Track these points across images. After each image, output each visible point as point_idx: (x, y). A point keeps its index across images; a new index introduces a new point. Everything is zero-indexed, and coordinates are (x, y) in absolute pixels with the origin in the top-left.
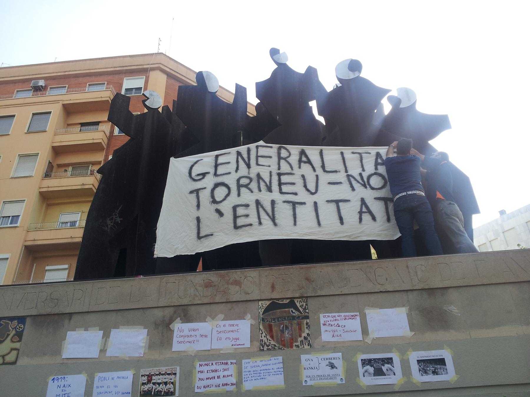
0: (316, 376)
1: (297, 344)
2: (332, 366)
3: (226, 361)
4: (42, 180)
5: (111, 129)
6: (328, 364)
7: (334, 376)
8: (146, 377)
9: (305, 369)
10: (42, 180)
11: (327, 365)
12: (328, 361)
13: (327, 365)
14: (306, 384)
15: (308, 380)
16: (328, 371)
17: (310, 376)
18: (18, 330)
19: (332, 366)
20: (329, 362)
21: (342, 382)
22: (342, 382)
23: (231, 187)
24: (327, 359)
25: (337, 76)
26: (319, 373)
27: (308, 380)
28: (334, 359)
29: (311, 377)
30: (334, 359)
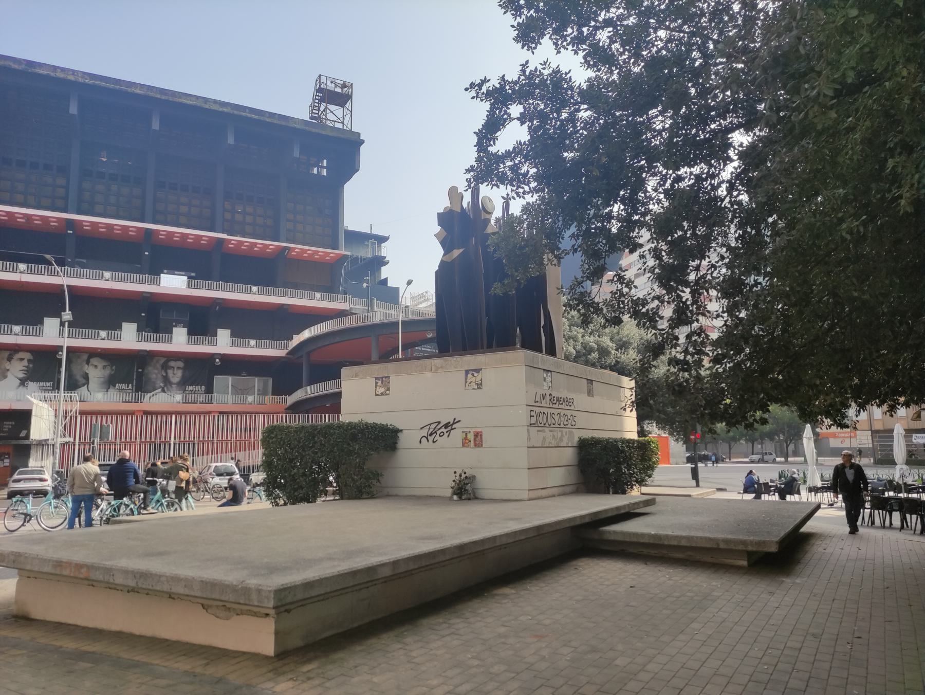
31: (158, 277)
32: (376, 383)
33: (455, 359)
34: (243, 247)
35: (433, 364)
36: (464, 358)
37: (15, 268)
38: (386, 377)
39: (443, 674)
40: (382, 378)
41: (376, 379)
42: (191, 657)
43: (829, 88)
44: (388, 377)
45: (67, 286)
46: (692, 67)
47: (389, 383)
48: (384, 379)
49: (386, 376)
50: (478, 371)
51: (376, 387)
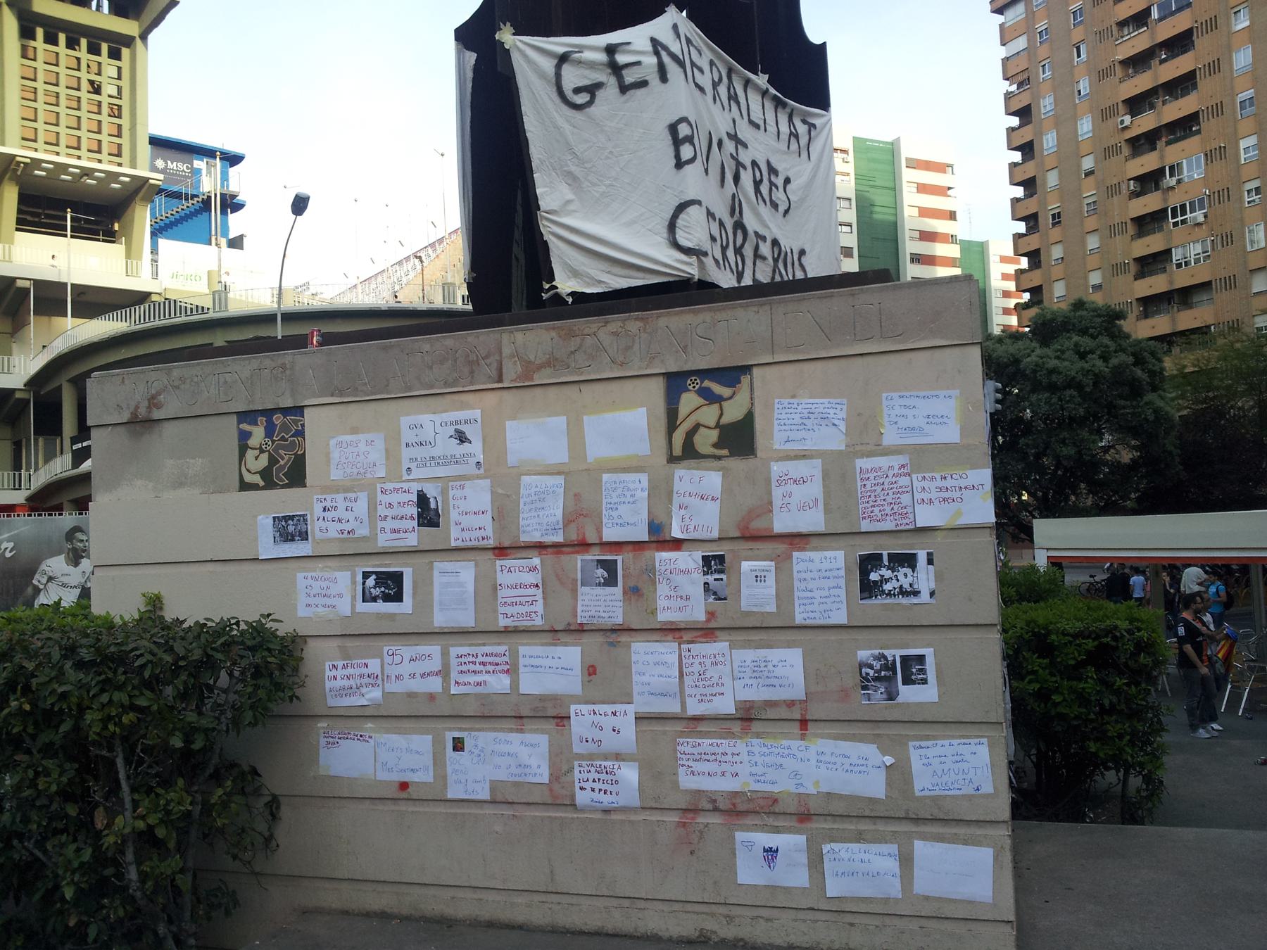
0: (428, 459)
1: (1099, 363)
2: (462, 438)
3: (363, 661)
4: (765, 130)
5: (598, 69)
6: (453, 433)
7: (467, 456)
8: (818, 462)
9: (407, 445)
10: (765, 130)
11: (451, 436)
12: (453, 428)
13: (451, 436)
14: (409, 475)
15: (413, 466)
16: (454, 447)
17: (416, 459)
18: (698, 381)
19: (462, 438)
20: (456, 430)
21: (479, 469)
22: (479, 469)
23: (530, 129)
24: (451, 424)
25: (147, 49)
26: (437, 452)
27: (413, 466)
28: (466, 422)
29: (419, 460)
30: (466, 422)
31: (139, 262)
32: (244, 436)
33: (613, 327)
34: (63, 177)
35: (506, 351)
36: (662, 322)
37: (217, 298)
38: (286, 411)
39: (666, 59)
40: (268, 413)
41: (246, 416)
42: (1093, 303)
43: (1236, 20)
44: (299, 410)
45: (72, 284)
46: (1053, 394)
47: (300, 433)
48: (278, 419)
49: (288, 403)
50: (732, 375)
51: (242, 455)
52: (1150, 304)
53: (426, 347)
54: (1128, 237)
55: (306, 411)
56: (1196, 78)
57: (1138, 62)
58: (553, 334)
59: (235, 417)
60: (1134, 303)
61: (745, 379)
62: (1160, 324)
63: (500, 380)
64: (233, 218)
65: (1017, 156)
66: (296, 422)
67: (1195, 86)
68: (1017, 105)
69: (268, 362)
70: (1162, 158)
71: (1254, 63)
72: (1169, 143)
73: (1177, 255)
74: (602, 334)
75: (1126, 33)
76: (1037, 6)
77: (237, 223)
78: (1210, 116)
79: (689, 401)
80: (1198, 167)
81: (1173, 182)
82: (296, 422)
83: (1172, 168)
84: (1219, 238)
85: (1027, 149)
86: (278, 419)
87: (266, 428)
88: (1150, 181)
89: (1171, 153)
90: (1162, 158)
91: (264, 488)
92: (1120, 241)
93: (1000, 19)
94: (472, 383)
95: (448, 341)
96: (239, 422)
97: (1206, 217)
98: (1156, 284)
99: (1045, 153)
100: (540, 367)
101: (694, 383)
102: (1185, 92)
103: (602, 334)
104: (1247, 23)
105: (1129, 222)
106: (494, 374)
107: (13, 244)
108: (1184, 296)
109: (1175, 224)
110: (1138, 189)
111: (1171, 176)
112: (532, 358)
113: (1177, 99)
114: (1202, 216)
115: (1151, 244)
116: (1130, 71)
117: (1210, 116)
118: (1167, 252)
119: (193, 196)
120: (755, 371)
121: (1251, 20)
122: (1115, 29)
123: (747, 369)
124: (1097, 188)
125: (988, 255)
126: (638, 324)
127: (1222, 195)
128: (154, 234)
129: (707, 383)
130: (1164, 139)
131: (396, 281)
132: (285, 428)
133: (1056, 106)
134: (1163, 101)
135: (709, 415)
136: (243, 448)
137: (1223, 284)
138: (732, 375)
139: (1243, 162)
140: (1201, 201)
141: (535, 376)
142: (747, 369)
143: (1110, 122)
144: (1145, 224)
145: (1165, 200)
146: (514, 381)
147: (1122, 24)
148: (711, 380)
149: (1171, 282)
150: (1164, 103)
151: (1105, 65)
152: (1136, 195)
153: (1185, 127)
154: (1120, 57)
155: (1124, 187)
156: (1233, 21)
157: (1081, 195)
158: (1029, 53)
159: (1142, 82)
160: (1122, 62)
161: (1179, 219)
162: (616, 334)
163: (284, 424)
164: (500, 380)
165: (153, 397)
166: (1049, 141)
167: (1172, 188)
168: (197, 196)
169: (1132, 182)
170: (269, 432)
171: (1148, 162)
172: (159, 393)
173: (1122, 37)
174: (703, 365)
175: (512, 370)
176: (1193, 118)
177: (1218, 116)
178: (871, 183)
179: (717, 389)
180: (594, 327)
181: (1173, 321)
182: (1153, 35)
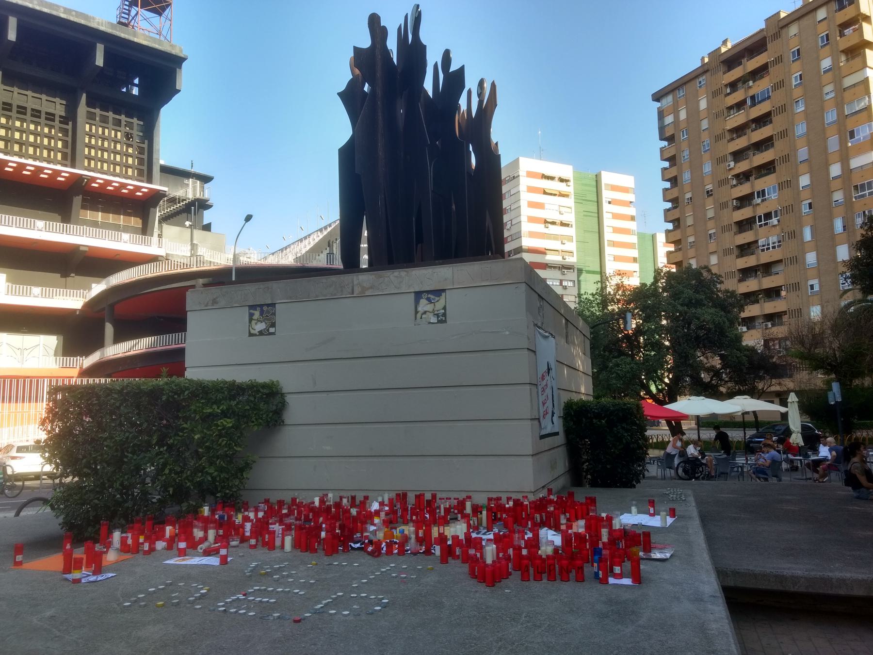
35: (355, 283)
38: (268, 305)
40: (261, 306)
44: (273, 305)
47: (274, 314)
50: (438, 293)
52: (746, 273)
53: (324, 281)
54: (732, 233)
55: (277, 305)
56: (773, 140)
57: (739, 131)
58: (373, 276)
59: (248, 307)
60: (736, 272)
61: (443, 294)
62: (751, 285)
63: (353, 294)
64: (206, 213)
65: (668, 185)
66: (272, 310)
67: (773, 145)
68: (667, 156)
69: (262, 286)
70: (752, 186)
71: (807, 131)
72: (756, 179)
73: (760, 243)
74: (392, 277)
75: (732, 113)
76: (679, 97)
77: (208, 216)
78: (782, 162)
79: (423, 302)
80: (775, 192)
81: (759, 201)
82: (272, 310)
83: (758, 193)
84: (787, 234)
85: (674, 181)
86: (265, 308)
87: (260, 312)
88: (745, 201)
89: (760, 184)
90: (752, 186)
91: (258, 336)
92: (728, 235)
93: (658, 105)
94: (342, 295)
95: (334, 278)
96: (249, 310)
97: (779, 221)
98: (750, 261)
99: (684, 183)
100: (368, 289)
101: (425, 296)
102: (767, 149)
103: (392, 277)
104: (803, 109)
105: (733, 224)
106: (350, 290)
107: (153, 236)
108: (767, 268)
109: (761, 226)
110: (739, 205)
111: (758, 197)
112: (365, 285)
113: (762, 152)
114: (777, 221)
115: (746, 237)
116: (735, 136)
117: (782, 162)
118: (757, 242)
119: (183, 200)
120: (447, 291)
121: (806, 107)
122: (725, 111)
123: (444, 290)
124: (714, 204)
125: (656, 242)
126: (405, 273)
127: (790, 209)
128: (160, 222)
129: (429, 296)
130: (754, 176)
131: (298, 251)
132: (268, 312)
133: (690, 156)
134: (753, 154)
135: (429, 307)
136: (251, 320)
137: (789, 261)
138: (438, 293)
139: (801, 189)
140: (776, 212)
141: (366, 292)
142: (444, 290)
143: (722, 165)
144: (744, 225)
145: (754, 212)
146: (358, 294)
147: (730, 108)
148: (431, 294)
149: (758, 260)
150: (754, 155)
151: (720, 132)
152: (737, 208)
153: (768, 168)
154: (728, 128)
155: (730, 203)
156: (795, 107)
157: (705, 207)
158: (675, 125)
159: (741, 143)
160: (729, 131)
161: (763, 222)
162: (396, 277)
163: (267, 310)
164: (353, 294)
165: (215, 299)
166: (687, 176)
167: (758, 204)
168: (185, 200)
169: (735, 201)
170: (261, 314)
171: (744, 189)
172: (217, 298)
173: (730, 116)
174: (428, 289)
175: (357, 290)
176: (772, 162)
177: (786, 162)
178: (584, 198)
179: (432, 297)
180: (389, 274)
181: (760, 282)
182: (748, 115)
